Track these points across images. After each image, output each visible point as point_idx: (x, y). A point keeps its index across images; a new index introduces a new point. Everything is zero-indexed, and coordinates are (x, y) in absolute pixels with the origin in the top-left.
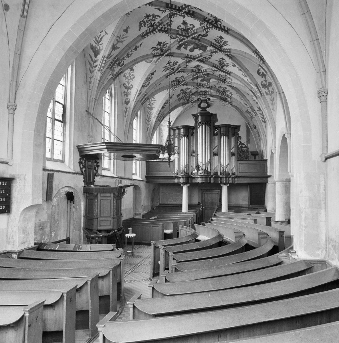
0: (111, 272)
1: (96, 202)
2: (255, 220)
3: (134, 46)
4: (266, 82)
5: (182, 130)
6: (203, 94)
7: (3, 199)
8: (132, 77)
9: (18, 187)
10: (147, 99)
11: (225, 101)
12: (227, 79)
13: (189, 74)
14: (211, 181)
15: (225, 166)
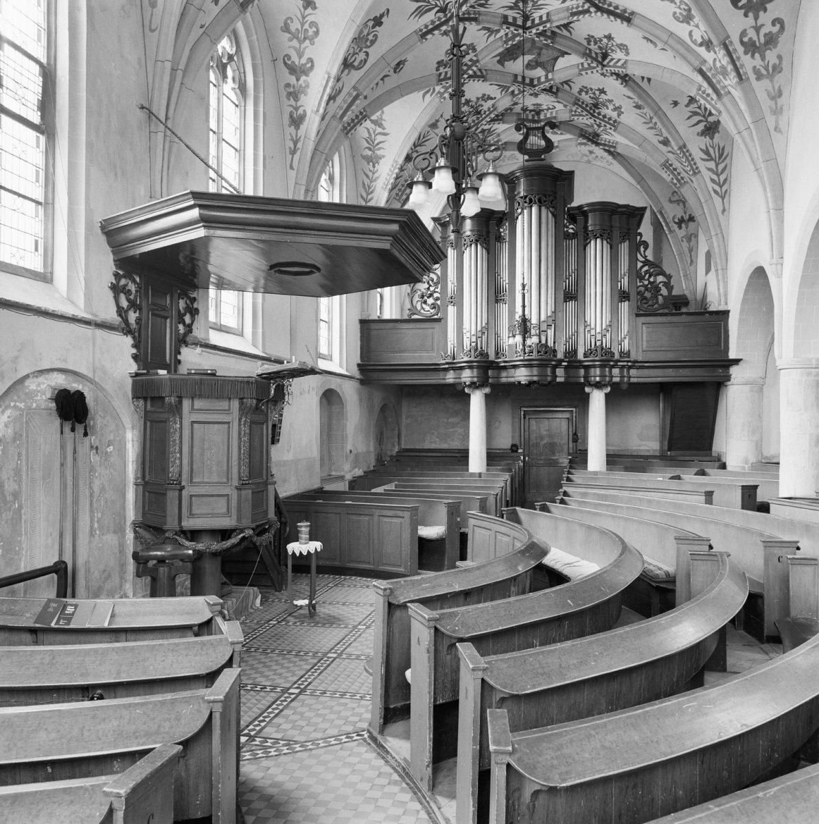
2: (709, 496)
4: (758, 35)
6: (530, 117)
8: (311, 32)
10: (360, 117)
12: (612, 51)
14: (556, 376)
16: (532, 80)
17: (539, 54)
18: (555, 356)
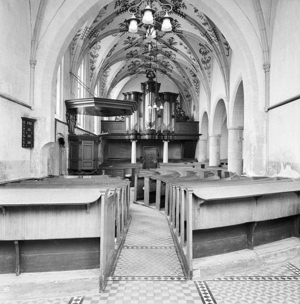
0: (103, 198)
1: (80, 147)
3: (108, 21)
5: (132, 96)
7: (29, 136)
8: (98, 48)
9: (39, 127)
11: (165, 74)
13: (142, 49)
15: (167, 126)
16: (150, 58)
17: (153, 53)
18: (155, 132)
